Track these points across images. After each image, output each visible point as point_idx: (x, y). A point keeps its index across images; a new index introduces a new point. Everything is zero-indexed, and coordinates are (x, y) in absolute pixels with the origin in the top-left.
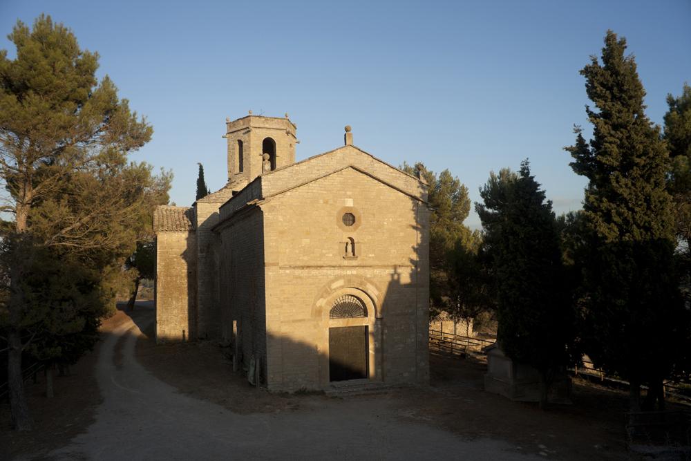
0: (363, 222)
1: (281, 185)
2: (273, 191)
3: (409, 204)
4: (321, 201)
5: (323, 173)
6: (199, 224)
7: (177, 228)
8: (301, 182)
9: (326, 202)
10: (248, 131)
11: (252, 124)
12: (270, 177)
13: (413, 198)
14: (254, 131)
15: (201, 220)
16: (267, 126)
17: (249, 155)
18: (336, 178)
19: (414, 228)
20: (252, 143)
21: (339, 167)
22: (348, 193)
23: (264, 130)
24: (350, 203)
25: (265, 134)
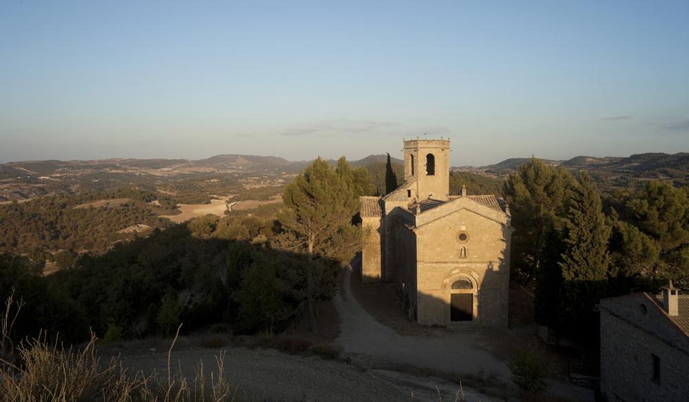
0: (471, 238)
1: (426, 220)
2: (422, 224)
3: (500, 227)
4: (447, 228)
5: (448, 213)
6: (387, 214)
7: (374, 214)
8: (436, 218)
9: (450, 228)
10: (416, 150)
12: (420, 216)
13: (502, 224)
14: (420, 151)
15: (388, 210)
16: (429, 146)
17: (417, 165)
18: (457, 215)
19: (503, 240)
20: (419, 157)
21: (458, 209)
22: (463, 223)
23: (427, 149)
24: (463, 228)
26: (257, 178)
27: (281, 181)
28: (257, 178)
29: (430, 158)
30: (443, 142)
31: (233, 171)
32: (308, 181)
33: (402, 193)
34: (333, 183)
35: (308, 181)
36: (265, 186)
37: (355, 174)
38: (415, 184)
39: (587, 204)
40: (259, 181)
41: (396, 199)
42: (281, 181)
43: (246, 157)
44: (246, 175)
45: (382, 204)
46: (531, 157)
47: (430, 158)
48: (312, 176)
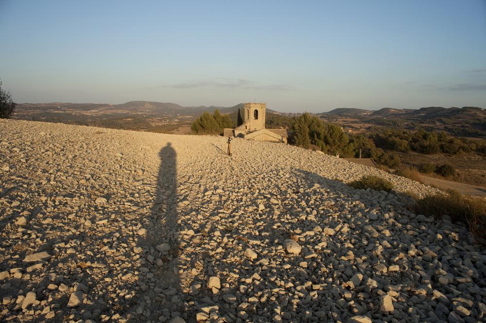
11: (251, 106)
14: (251, 108)
18: (261, 136)
25: (255, 109)
26: (160, 118)
27: (176, 120)
28: (160, 118)
29: (256, 112)
30: (262, 105)
31: (143, 113)
32: (201, 121)
33: (243, 127)
34: (211, 122)
35: (201, 121)
36: (166, 124)
37: (223, 118)
38: (249, 123)
39: (302, 131)
40: (161, 121)
41: (240, 130)
42: (176, 120)
43: (151, 103)
44: (152, 116)
45: (234, 132)
46: (305, 112)
47: (256, 112)
48: (203, 119)
